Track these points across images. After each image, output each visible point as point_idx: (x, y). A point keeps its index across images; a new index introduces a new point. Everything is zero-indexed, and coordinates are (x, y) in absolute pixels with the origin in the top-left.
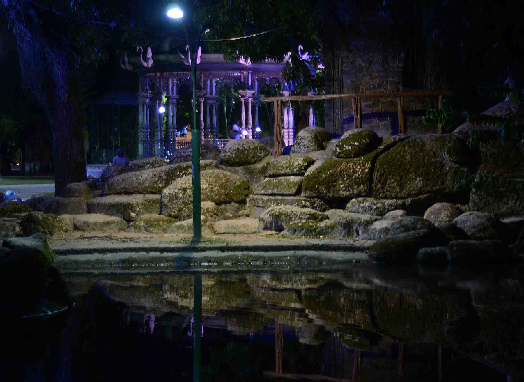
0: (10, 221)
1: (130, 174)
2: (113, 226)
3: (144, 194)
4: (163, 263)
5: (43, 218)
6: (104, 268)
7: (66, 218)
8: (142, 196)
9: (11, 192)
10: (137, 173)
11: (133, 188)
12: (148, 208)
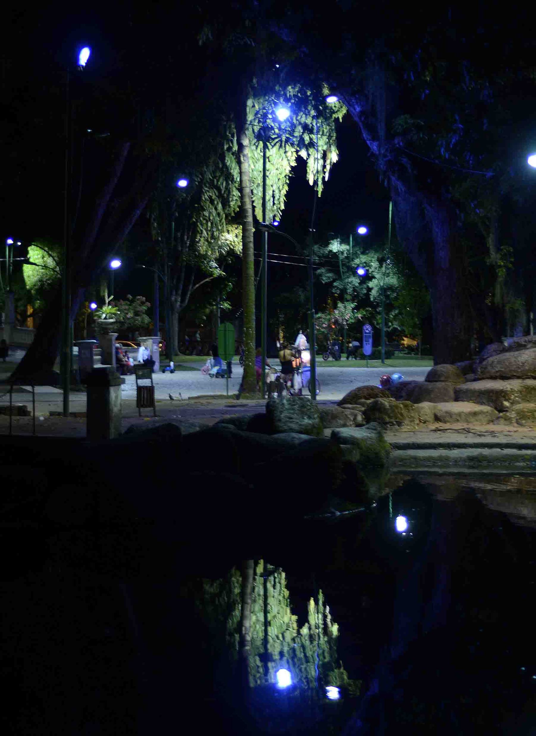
0: (353, 409)
1: (508, 355)
2: (480, 417)
3: (524, 379)
4: (519, 462)
5: (390, 406)
6: (448, 466)
7: (426, 406)
8: (520, 381)
9: (400, 375)
10: (517, 353)
11: (511, 371)
12: (526, 396)
